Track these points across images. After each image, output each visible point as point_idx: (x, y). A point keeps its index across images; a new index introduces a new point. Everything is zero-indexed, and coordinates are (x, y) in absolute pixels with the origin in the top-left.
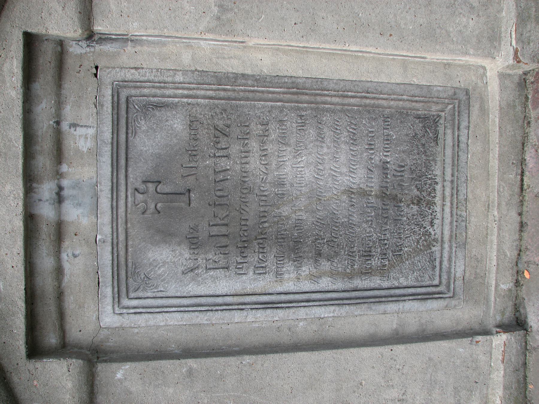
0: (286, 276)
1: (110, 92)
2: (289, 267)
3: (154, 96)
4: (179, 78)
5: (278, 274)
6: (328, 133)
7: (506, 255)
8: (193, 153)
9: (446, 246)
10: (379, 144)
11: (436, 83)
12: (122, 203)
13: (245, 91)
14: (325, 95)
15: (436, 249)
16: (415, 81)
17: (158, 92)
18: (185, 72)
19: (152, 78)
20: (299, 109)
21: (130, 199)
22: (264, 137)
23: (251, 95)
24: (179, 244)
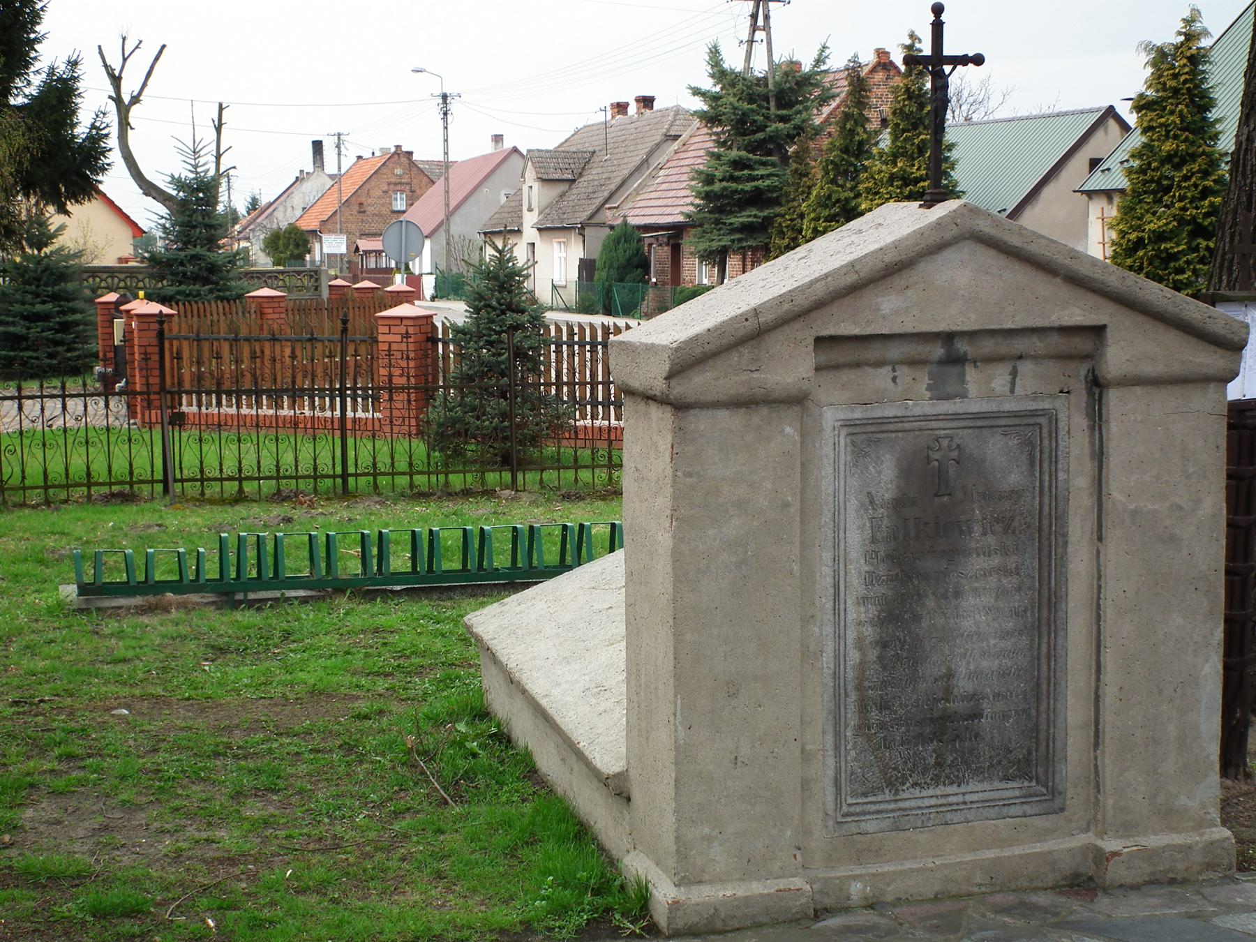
0: (863, 609)
1: (1047, 407)
2: (873, 611)
3: (1041, 451)
4: (1062, 476)
5: (865, 600)
6: (1009, 644)
7: (888, 885)
8: (990, 496)
9: (892, 806)
10: (1000, 705)
11: (1070, 768)
12: (941, 424)
13: (1050, 546)
14: (1049, 633)
15: (888, 796)
16: (1070, 741)
17: (1046, 456)
18: (1067, 481)
19: (1061, 448)
20: (1033, 608)
21: (943, 432)
22: (1004, 571)
23: (1045, 553)
24: (898, 487)
